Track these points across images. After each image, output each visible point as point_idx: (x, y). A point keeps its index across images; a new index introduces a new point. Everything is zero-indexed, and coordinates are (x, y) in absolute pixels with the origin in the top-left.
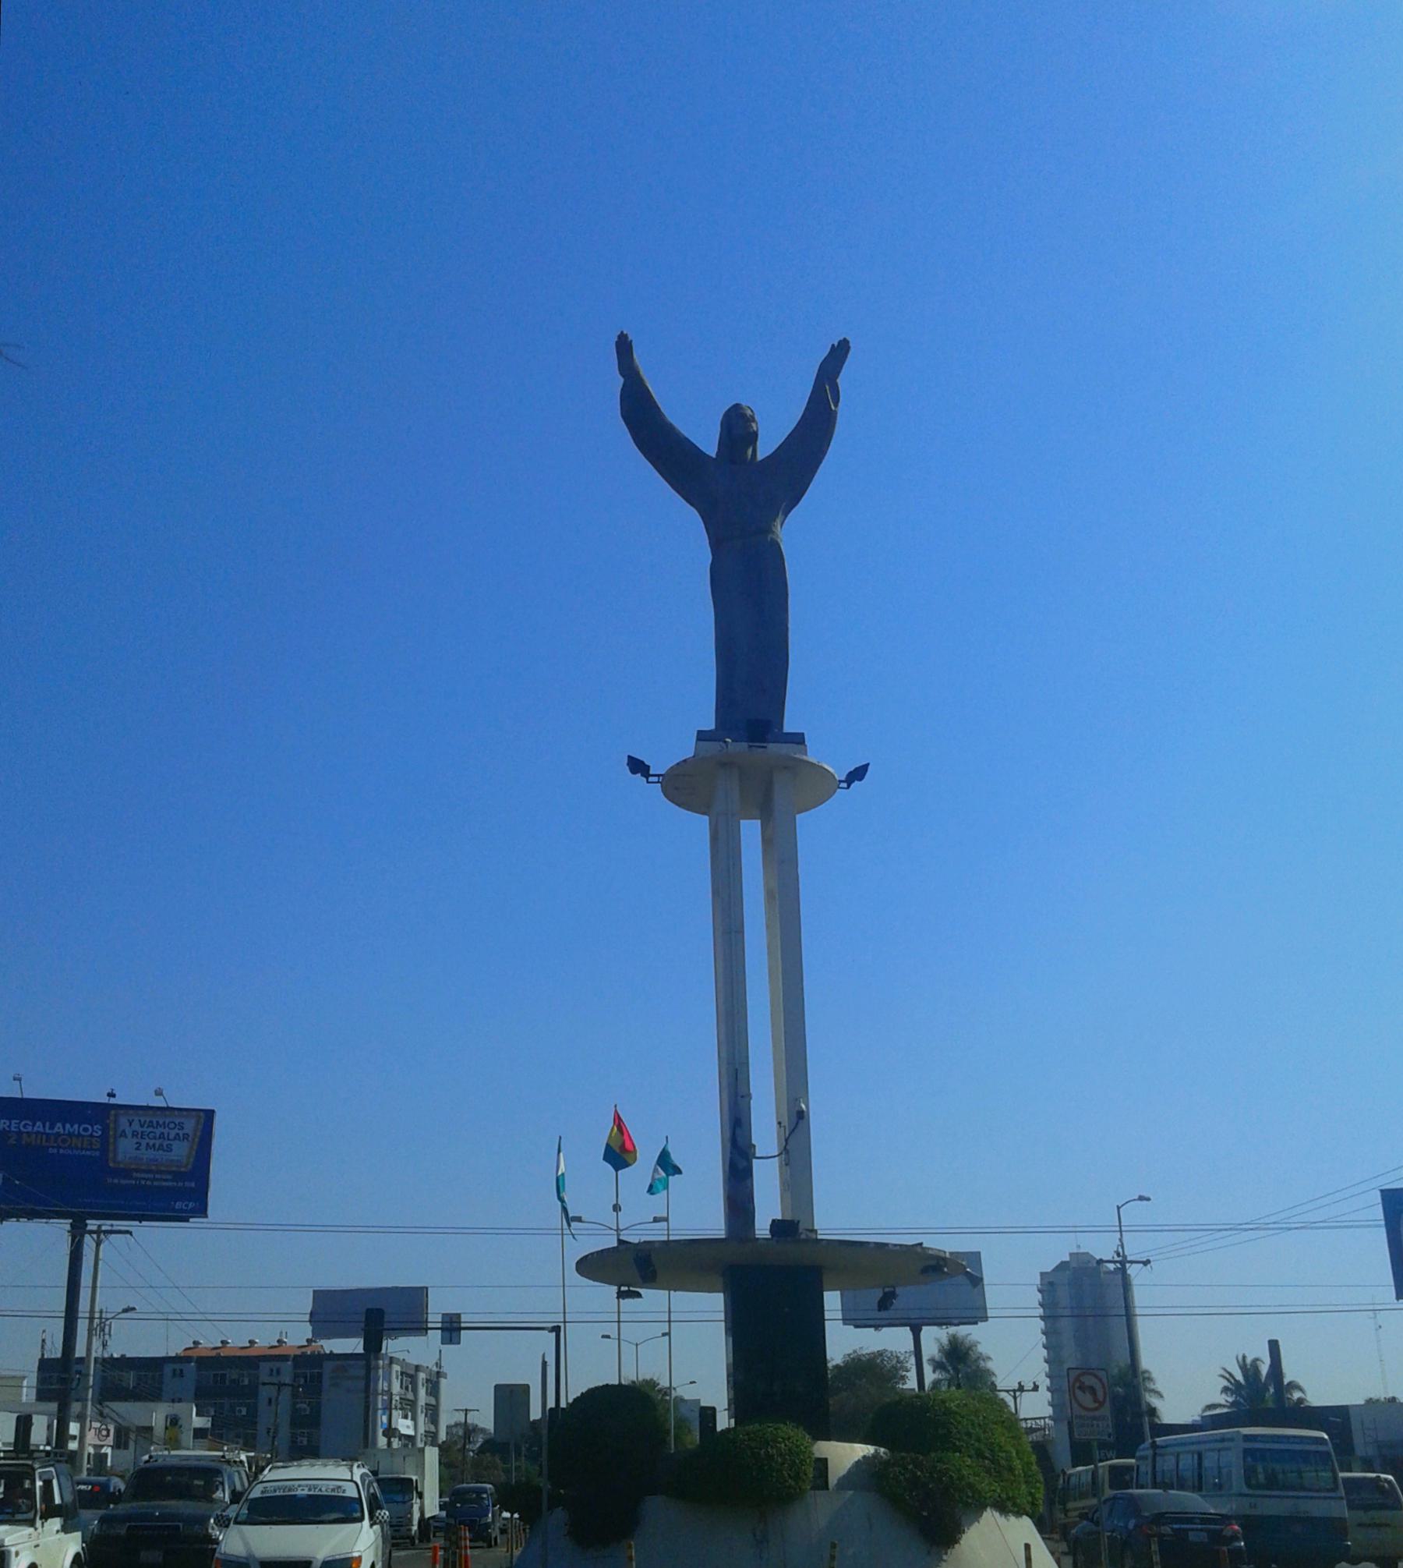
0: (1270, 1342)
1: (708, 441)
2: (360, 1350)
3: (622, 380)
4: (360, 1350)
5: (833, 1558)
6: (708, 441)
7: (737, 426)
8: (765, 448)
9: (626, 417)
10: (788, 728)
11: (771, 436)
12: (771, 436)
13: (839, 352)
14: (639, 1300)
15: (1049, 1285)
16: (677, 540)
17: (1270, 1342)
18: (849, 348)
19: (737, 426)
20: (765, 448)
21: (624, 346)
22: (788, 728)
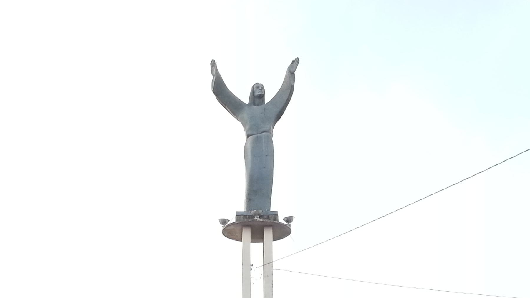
1: (245, 98)
6: (245, 98)
19: (257, 95)
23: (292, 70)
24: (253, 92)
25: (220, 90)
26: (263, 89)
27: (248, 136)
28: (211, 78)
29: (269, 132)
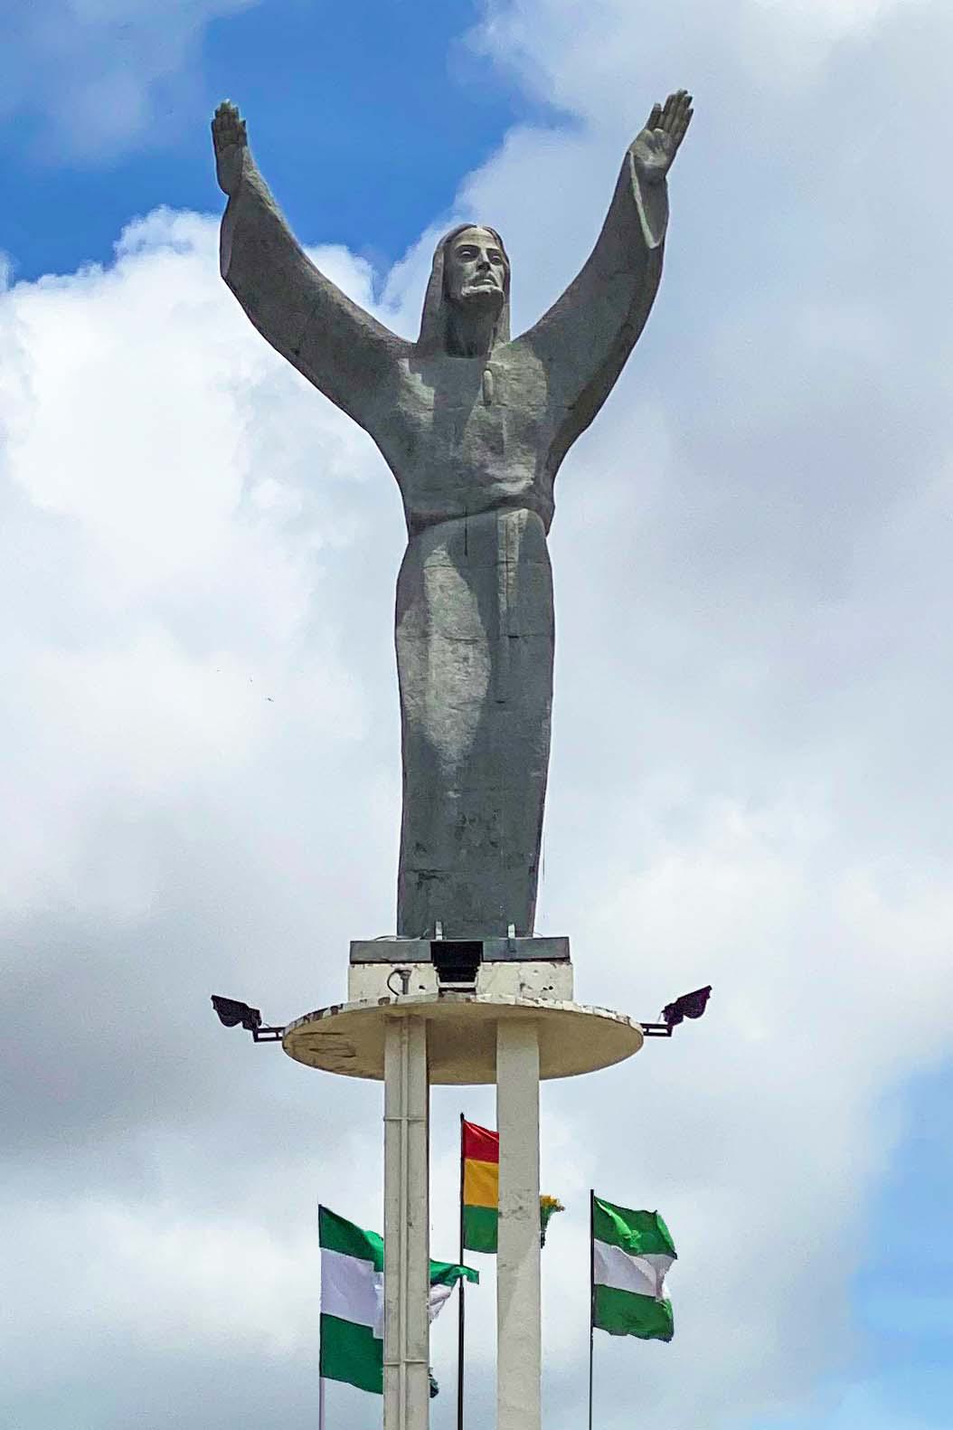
22: (541, 930)
23: (651, 160)
27: (417, 525)
29: (541, 503)
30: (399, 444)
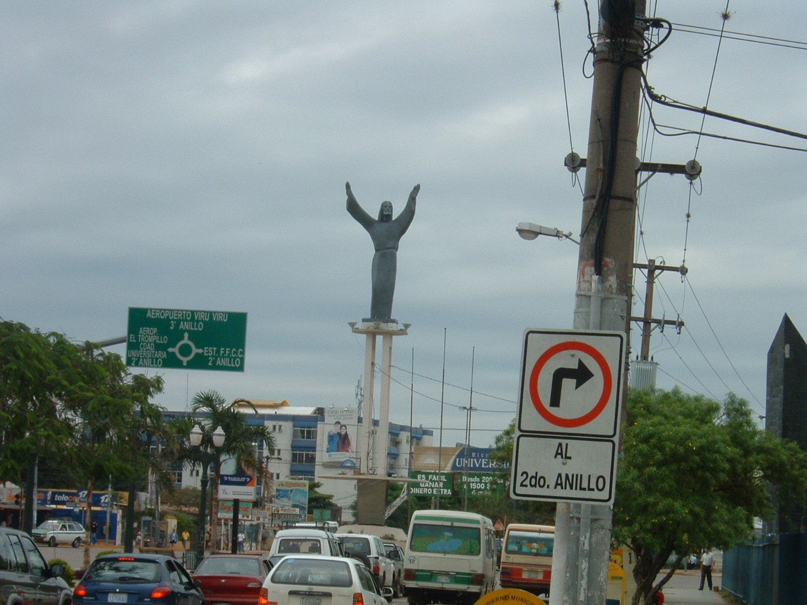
0: (363, 321)
1: (375, 215)
2: (221, 488)
3: (347, 197)
4: (221, 488)
5: (412, 380)
6: (375, 215)
7: (386, 209)
8: (395, 216)
9: (348, 210)
10: (392, 317)
11: (397, 211)
12: (397, 211)
13: (417, 189)
14: (787, 313)
15: (196, 353)
16: (363, 243)
17: (363, 321)
18: (420, 188)
19: (386, 209)
20: (395, 216)
21: (348, 186)
22: (392, 317)
24: (382, 211)
25: (354, 208)
26: (391, 207)
28: (346, 197)
30: (374, 237)
